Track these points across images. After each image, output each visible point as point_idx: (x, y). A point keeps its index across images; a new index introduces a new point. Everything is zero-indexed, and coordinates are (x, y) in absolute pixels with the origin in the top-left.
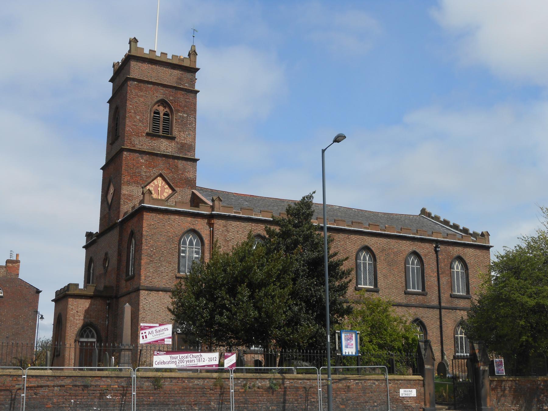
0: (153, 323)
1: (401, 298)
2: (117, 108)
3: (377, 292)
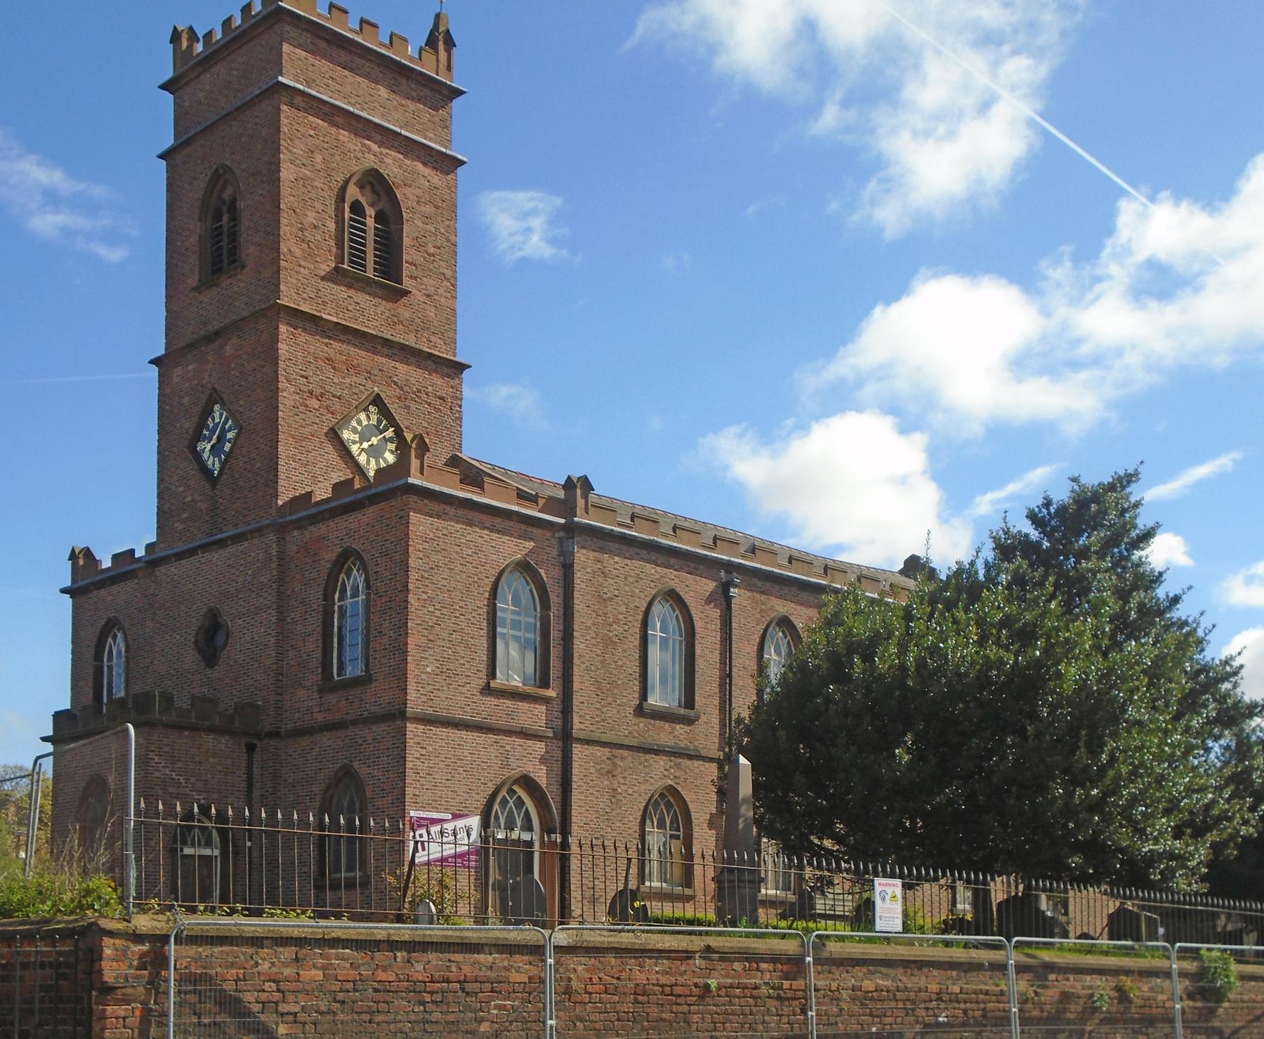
0: (437, 810)
1: (632, 729)
2: (220, 177)
3: (689, 721)
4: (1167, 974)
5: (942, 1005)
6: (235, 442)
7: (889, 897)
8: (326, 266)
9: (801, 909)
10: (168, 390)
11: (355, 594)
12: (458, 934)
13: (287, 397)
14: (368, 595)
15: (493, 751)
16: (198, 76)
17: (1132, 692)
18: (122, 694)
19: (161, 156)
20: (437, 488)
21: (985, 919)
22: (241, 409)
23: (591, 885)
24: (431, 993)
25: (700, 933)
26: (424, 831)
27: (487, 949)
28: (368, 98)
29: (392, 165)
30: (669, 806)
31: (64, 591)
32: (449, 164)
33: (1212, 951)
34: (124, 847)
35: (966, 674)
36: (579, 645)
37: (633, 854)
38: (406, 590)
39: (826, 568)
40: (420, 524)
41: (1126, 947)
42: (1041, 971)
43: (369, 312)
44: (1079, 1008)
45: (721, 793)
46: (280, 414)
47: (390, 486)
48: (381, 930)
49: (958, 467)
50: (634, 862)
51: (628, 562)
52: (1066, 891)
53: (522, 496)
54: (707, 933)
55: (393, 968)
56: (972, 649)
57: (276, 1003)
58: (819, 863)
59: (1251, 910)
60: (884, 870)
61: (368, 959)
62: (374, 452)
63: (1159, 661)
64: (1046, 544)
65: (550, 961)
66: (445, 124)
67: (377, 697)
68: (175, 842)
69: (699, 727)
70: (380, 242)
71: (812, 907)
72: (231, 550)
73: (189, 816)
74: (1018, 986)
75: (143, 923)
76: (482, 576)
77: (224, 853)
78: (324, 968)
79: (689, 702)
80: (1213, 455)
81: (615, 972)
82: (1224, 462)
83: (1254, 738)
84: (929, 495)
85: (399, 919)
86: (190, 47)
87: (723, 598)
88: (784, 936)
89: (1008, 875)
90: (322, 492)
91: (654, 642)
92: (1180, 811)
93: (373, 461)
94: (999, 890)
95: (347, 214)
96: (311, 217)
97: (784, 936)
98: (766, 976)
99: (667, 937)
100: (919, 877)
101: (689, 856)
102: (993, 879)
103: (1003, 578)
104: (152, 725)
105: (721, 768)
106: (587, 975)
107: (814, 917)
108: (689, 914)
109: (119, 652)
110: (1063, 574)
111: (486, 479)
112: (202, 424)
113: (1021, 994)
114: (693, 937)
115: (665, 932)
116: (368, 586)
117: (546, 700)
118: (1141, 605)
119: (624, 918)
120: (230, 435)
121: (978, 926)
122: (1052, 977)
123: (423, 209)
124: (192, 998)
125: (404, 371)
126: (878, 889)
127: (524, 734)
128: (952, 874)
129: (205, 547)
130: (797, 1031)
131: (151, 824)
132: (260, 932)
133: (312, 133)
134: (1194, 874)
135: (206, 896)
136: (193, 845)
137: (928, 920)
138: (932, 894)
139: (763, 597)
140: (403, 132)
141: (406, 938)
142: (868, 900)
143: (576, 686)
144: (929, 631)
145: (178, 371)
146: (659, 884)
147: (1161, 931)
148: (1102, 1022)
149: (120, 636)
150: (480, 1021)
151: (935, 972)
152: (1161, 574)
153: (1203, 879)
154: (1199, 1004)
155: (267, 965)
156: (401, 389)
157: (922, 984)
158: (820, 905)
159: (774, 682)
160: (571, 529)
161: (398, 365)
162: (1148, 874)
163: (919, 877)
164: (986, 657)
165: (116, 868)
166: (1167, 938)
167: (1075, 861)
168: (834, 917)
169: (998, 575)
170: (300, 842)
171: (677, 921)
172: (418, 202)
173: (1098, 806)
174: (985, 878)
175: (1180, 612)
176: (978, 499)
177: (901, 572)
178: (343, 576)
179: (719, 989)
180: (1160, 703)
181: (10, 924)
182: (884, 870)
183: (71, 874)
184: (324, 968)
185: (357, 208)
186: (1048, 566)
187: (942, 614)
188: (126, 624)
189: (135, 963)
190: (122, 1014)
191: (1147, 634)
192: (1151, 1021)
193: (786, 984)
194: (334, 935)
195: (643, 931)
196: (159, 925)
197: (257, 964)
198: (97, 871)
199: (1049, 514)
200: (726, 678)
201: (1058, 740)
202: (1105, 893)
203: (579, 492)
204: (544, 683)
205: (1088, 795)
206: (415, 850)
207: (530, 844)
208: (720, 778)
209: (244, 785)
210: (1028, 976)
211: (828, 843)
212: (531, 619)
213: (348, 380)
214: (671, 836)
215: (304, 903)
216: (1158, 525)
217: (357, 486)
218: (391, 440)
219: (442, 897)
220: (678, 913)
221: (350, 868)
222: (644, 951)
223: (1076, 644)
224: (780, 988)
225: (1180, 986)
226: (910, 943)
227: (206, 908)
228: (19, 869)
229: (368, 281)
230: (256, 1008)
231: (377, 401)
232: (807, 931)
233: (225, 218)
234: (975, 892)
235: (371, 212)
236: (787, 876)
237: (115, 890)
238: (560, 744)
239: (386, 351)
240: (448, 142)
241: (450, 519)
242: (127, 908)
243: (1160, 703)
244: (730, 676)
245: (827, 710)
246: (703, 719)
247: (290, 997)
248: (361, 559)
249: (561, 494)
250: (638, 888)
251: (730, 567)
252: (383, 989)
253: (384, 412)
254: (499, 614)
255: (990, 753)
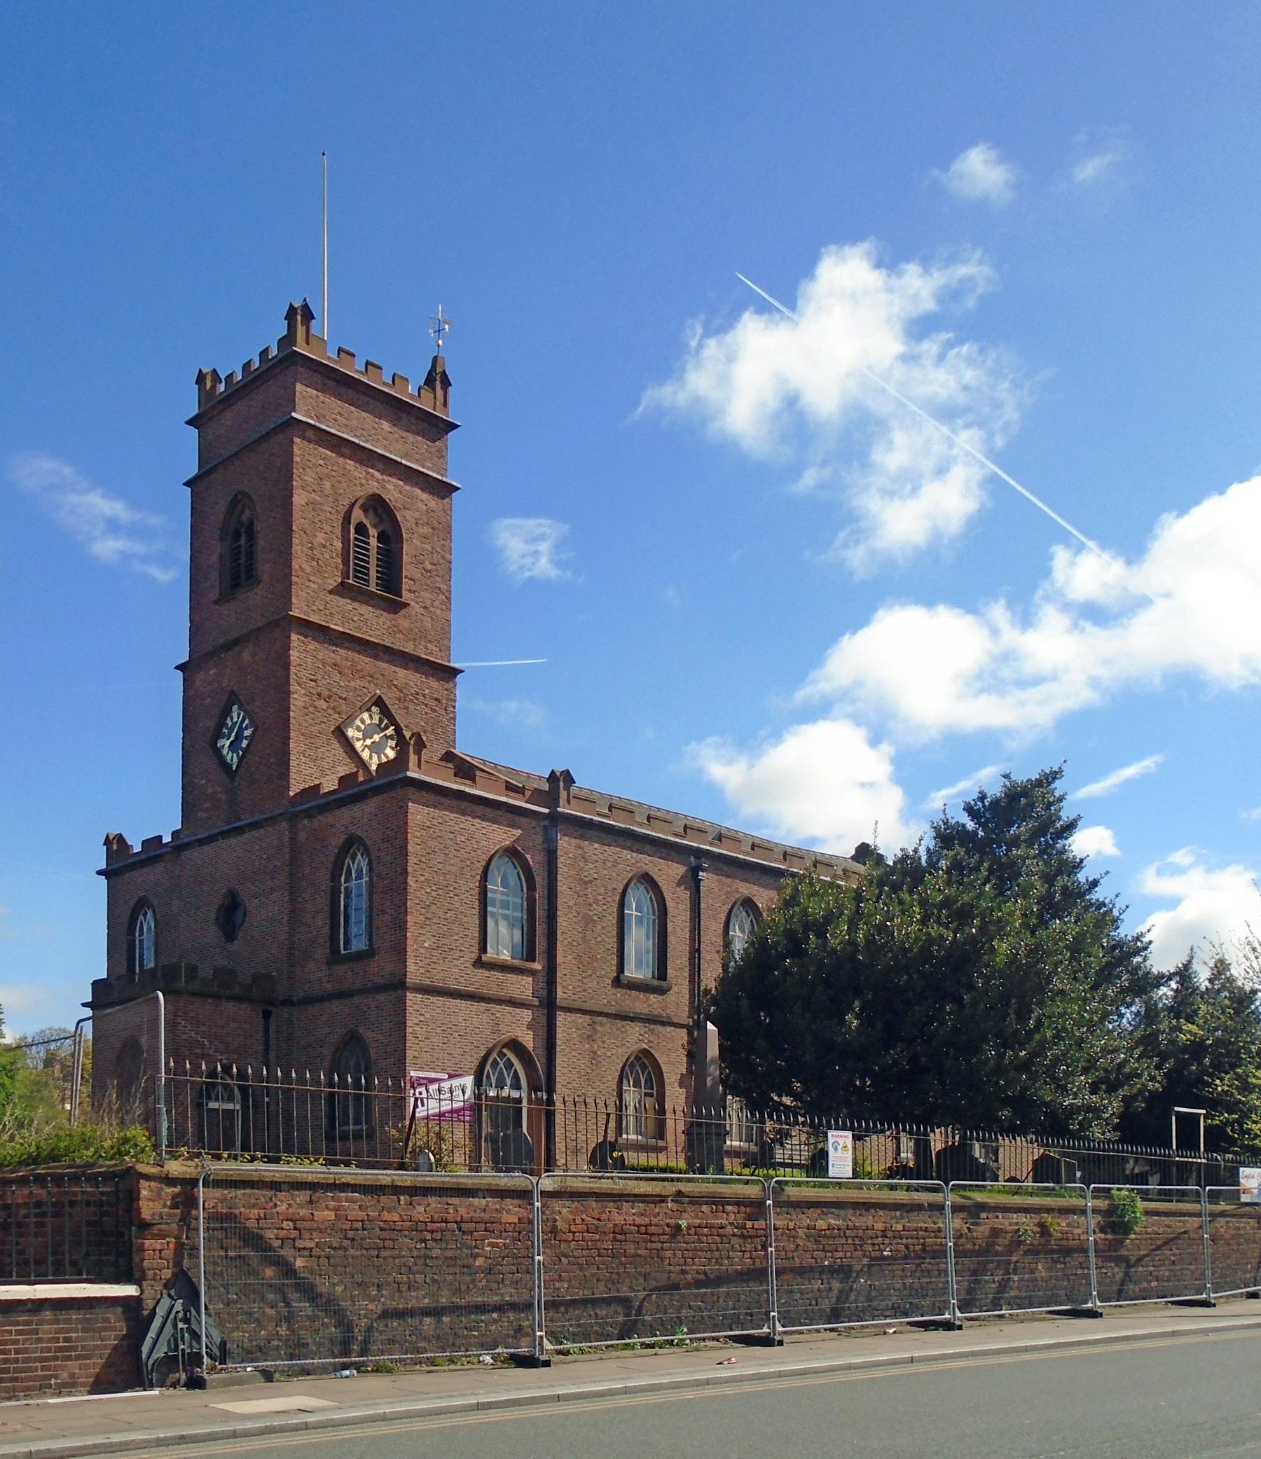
2: (238, 501)
3: (662, 991)
4: (1083, 1212)
5: (887, 1241)
6: (251, 738)
7: (841, 1149)
8: (334, 581)
9: (762, 1158)
10: (191, 694)
11: (359, 877)
12: (455, 1180)
13: (298, 699)
14: (371, 878)
15: (485, 1018)
16: (222, 411)
17: (1056, 965)
18: (152, 965)
19: (186, 484)
20: (433, 781)
21: (925, 1165)
22: (257, 710)
23: (573, 1137)
24: (432, 1232)
25: (672, 1180)
26: (423, 1089)
27: (480, 1194)
28: (373, 431)
29: (393, 490)
30: (644, 1067)
31: (99, 873)
32: (444, 490)
33: (1122, 1191)
34: (157, 1101)
35: (911, 950)
36: (562, 923)
37: (612, 1110)
38: (405, 873)
39: (785, 854)
40: (418, 814)
41: (1047, 1188)
42: (974, 1210)
43: (369, 622)
44: (1007, 1242)
45: (690, 1055)
46: (292, 714)
47: (391, 779)
48: (386, 1176)
49: (914, 768)
50: (613, 1116)
51: (606, 848)
52: (997, 1139)
53: (510, 788)
54: (678, 1180)
55: (396, 1211)
56: (915, 927)
57: (294, 1240)
58: (779, 1117)
59: (1155, 1155)
60: (837, 1122)
61: (374, 1202)
62: (376, 748)
63: (1080, 938)
64: (981, 833)
65: (538, 1204)
66: (441, 455)
67: (380, 969)
68: (201, 1097)
69: (671, 997)
70: (381, 560)
71: (772, 1156)
72: (247, 836)
73: (212, 1074)
74: (955, 1223)
75: (175, 1168)
76: (475, 861)
77: (245, 1108)
78: (336, 1209)
79: (662, 973)
80: (1140, 758)
81: (596, 1214)
82: (1148, 763)
83: (1160, 1005)
84: (895, 797)
85: (402, 1167)
86: (213, 387)
87: (692, 882)
88: (747, 1182)
89: (946, 1127)
90: (329, 785)
91: (630, 920)
92: (1096, 1070)
93: (375, 756)
94: (937, 1140)
95: (352, 536)
96: (320, 538)
97: (747, 1182)
98: (729, 1218)
99: (643, 1183)
100: (867, 1129)
101: (662, 1111)
102: (932, 1131)
103: (943, 863)
104: (179, 993)
105: (690, 1034)
106: (570, 1217)
107: (774, 1166)
108: (662, 1164)
109: (149, 928)
110: (996, 860)
111: (478, 773)
112: (222, 724)
113: (956, 1231)
114: (666, 1183)
115: (641, 1179)
116: (371, 869)
117: (532, 973)
118: (1065, 888)
119: (604, 1166)
120: (247, 733)
121: (920, 1170)
122: (984, 1215)
123: (421, 530)
124: (219, 1234)
125: (403, 675)
126: (831, 1140)
127: (512, 1002)
128: (897, 1126)
129: (224, 834)
130: (758, 1264)
131: (179, 1081)
132: (278, 1177)
133: (322, 462)
134: (1107, 1124)
135: (229, 1145)
136: (217, 1100)
137: (875, 1167)
138: (881, 1147)
139: (729, 880)
140: (404, 462)
141: (408, 1184)
142: (822, 1149)
143: (559, 959)
144: (876, 912)
145: (201, 675)
146: (634, 1137)
147: (1078, 1174)
148: (1026, 1253)
149: (150, 913)
150: (475, 1257)
151: (881, 1213)
152: (1082, 861)
153: (1115, 1128)
154: (1109, 1237)
155: (284, 1207)
156: (401, 691)
157: (870, 1223)
158: (779, 1155)
159: (737, 957)
160: (556, 819)
161: (398, 669)
162: (1068, 1125)
163: (867, 1129)
164: (928, 934)
165: (150, 1119)
166: (1083, 1181)
167: (1005, 1113)
168: (792, 1166)
169: (938, 861)
170: (313, 1099)
171: (651, 1169)
172: (417, 524)
173: (1025, 1066)
174: (925, 1129)
175: (1099, 894)
176: (933, 795)
177: (853, 858)
178: (348, 860)
179: (689, 1228)
180: (1080, 975)
181: (58, 1167)
182: (837, 1122)
183: (111, 1125)
184: (336, 1209)
185: (361, 529)
186: (983, 854)
187: (889, 896)
188: (155, 903)
189: (169, 1203)
190: (159, 1247)
191: (1069, 914)
192: (1068, 1252)
193: (749, 1224)
194: (344, 1180)
195: (621, 1178)
196: (189, 1170)
197: (276, 1205)
198: (133, 1122)
199: (984, 806)
200: (695, 953)
201: (991, 1008)
202: (1031, 1142)
203: (562, 784)
204: (531, 957)
205: (1017, 1056)
206: (416, 1106)
207: (519, 1101)
208: (689, 1043)
209: (262, 1047)
210: (962, 1215)
211: (787, 1100)
212: (518, 900)
213: (352, 684)
214: (646, 1094)
215: (317, 1152)
216: (1080, 817)
217: (361, 779)
218: (391, 737)
219: (440, 1148)
220: (653, 1163)
221: (357, 1121)
222: (621, 1195)
223: (1008, 923)
224: (744, 1227)
225: (1093, 1221)
226: (859, 1187)
227: (229, 1156)
228: (67, 1119)
229: (371, 595)
230: (277, 1243)
231: (379, 702)
232: (770, 1178)
233: (243, 540)
234: (917, 1143)
235: (373, 532)
236: (749, 1129)
237: (149, 1139)
238: (545, 1011)
239: (386, 657)
240: (444, 471)
241: (445, 809)
242: (160, 1155)
243: (1080, 975)
244: (699, 951)
245: (785, 981)
246: (675, 989)
247: (306, 1235)
248: (364, 844)
249: (546, 787)
250: (616, 1140)
251: (698, 853)
252: (389, 1228)
253: (385, 712)
254: (489, 895)
255: (931, 1020)
